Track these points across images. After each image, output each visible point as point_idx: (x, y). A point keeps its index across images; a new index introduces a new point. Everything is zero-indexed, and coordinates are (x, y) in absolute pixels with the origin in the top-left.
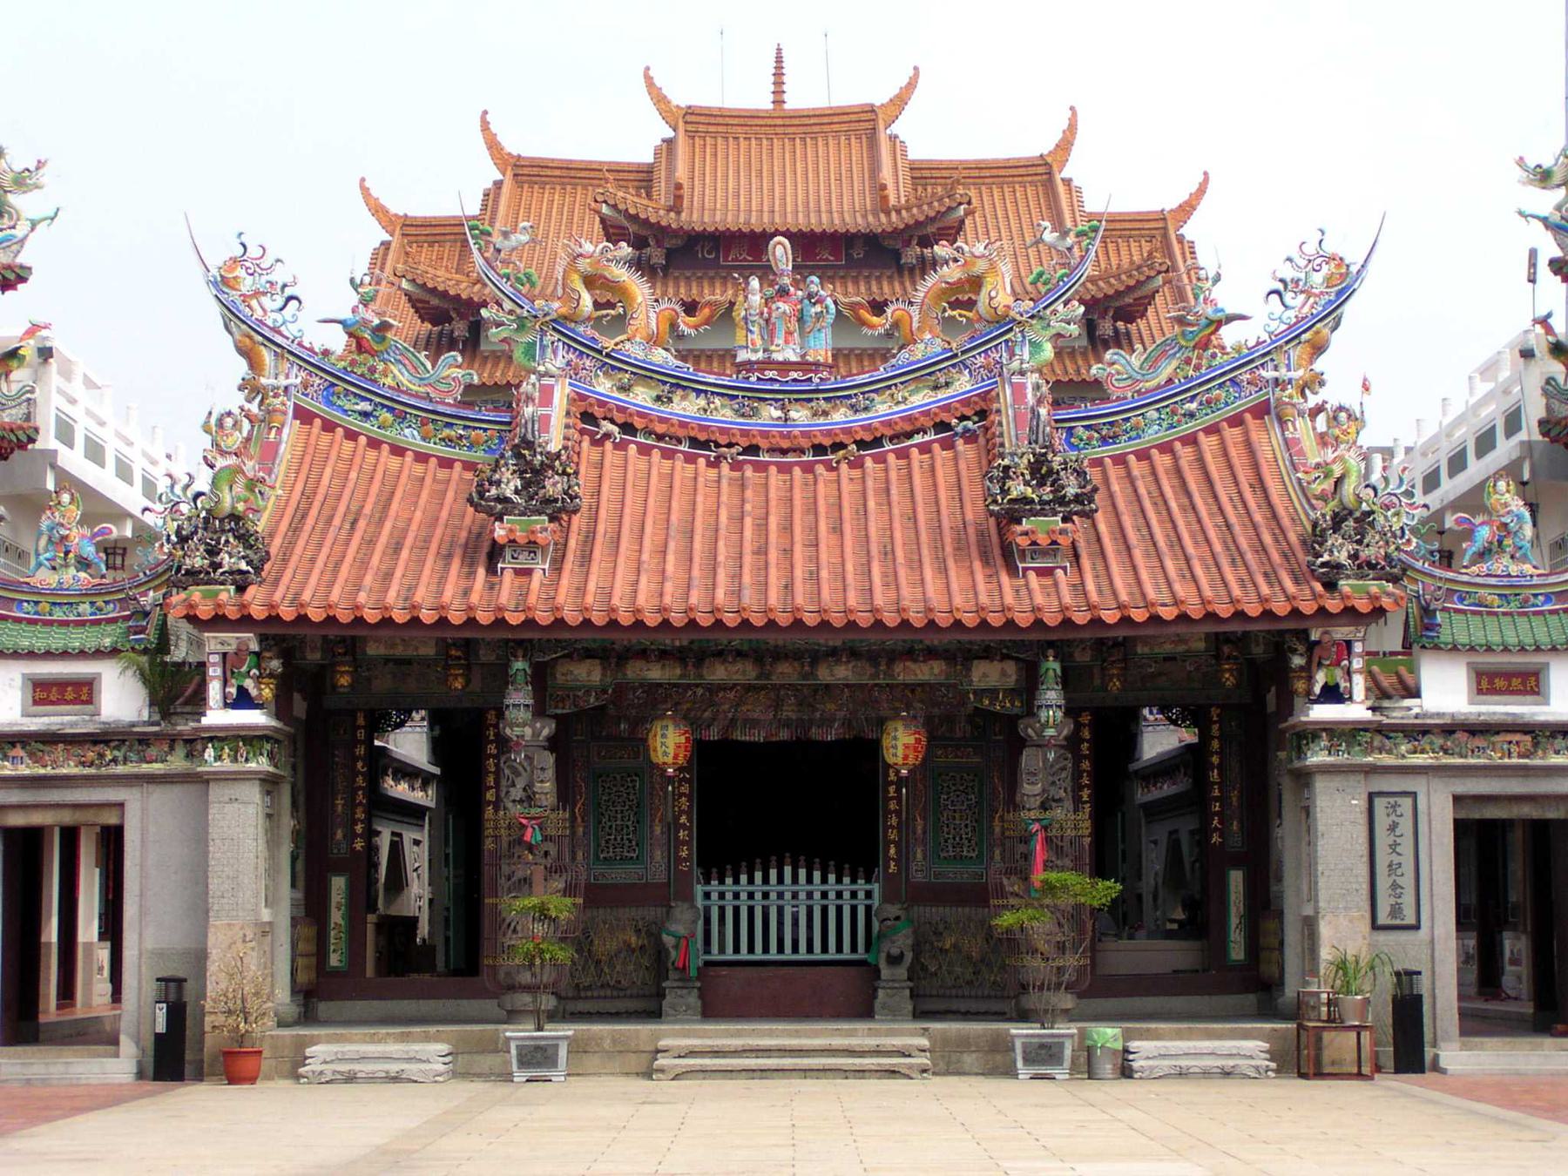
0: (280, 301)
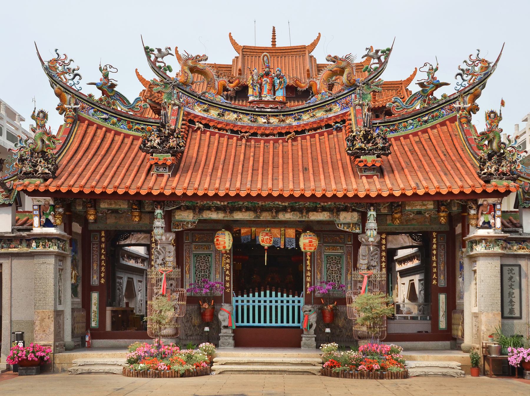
0: (72, 76)
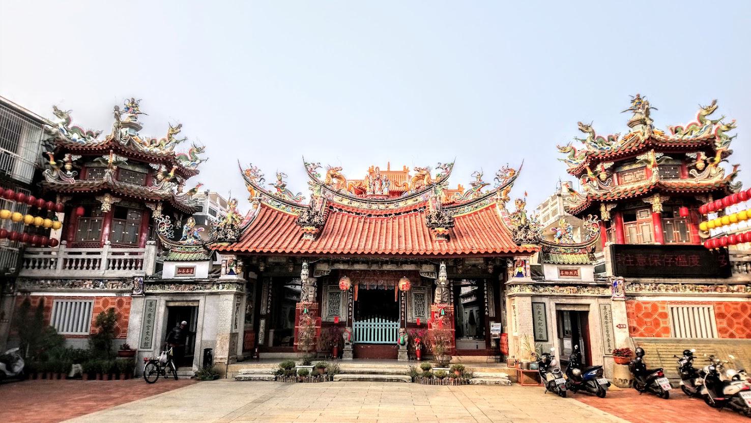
0: (259, 179)
